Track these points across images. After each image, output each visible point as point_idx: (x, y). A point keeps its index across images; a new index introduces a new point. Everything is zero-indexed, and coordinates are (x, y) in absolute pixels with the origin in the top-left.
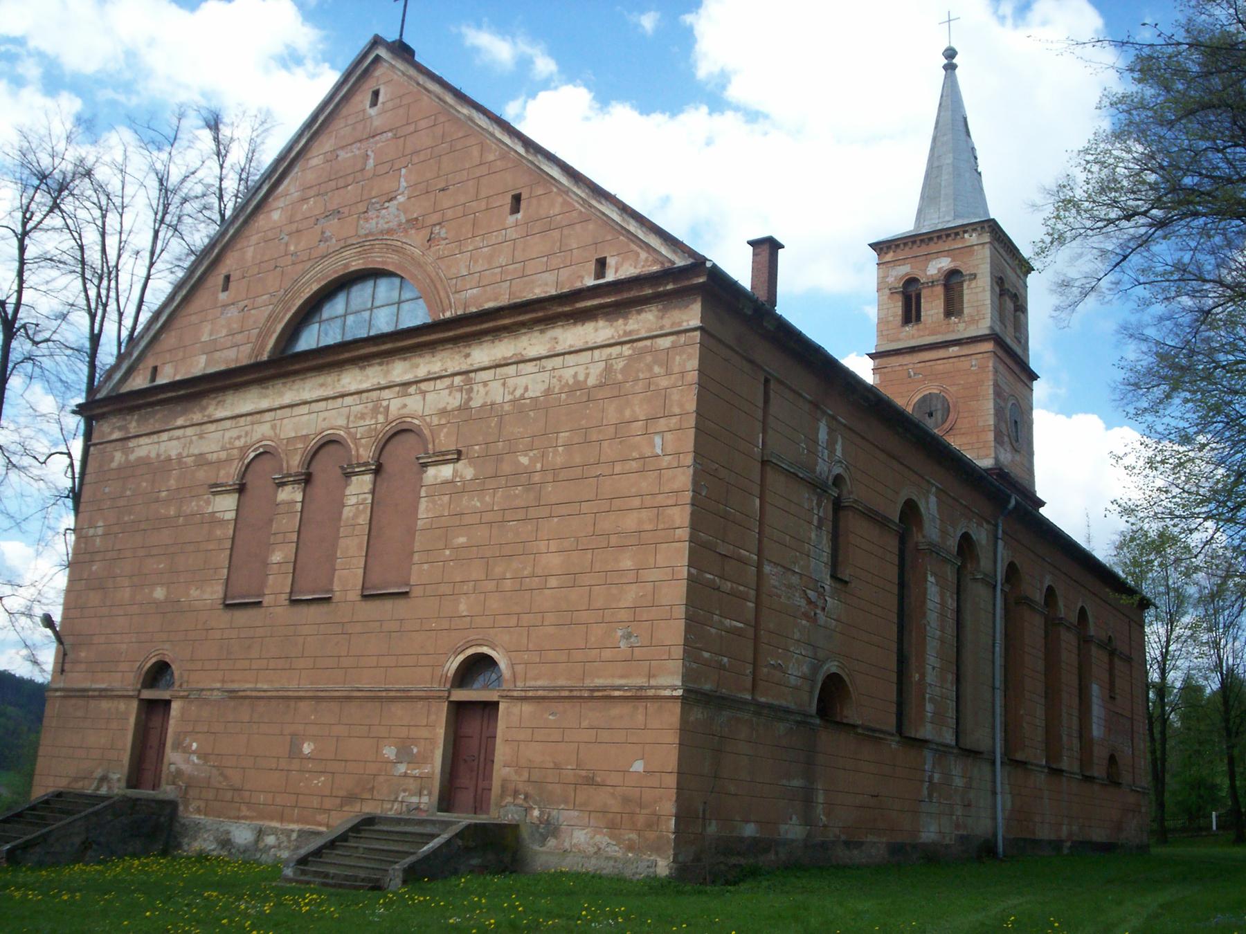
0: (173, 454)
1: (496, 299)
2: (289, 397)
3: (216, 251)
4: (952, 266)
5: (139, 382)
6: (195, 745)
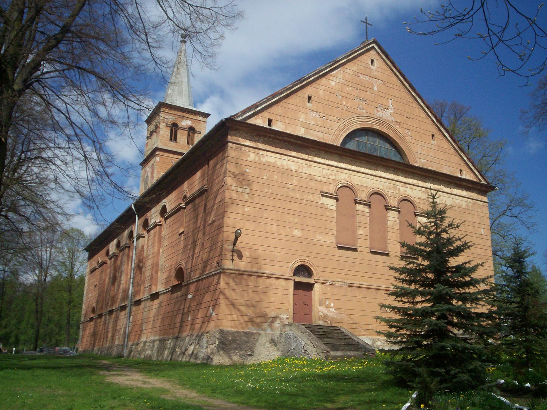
0: (293, 168)
1: (432, 167)
2: (410, 181)
3: (305, 83)
4: (192, 125)
5: (260, 121)
6: (332, 305)
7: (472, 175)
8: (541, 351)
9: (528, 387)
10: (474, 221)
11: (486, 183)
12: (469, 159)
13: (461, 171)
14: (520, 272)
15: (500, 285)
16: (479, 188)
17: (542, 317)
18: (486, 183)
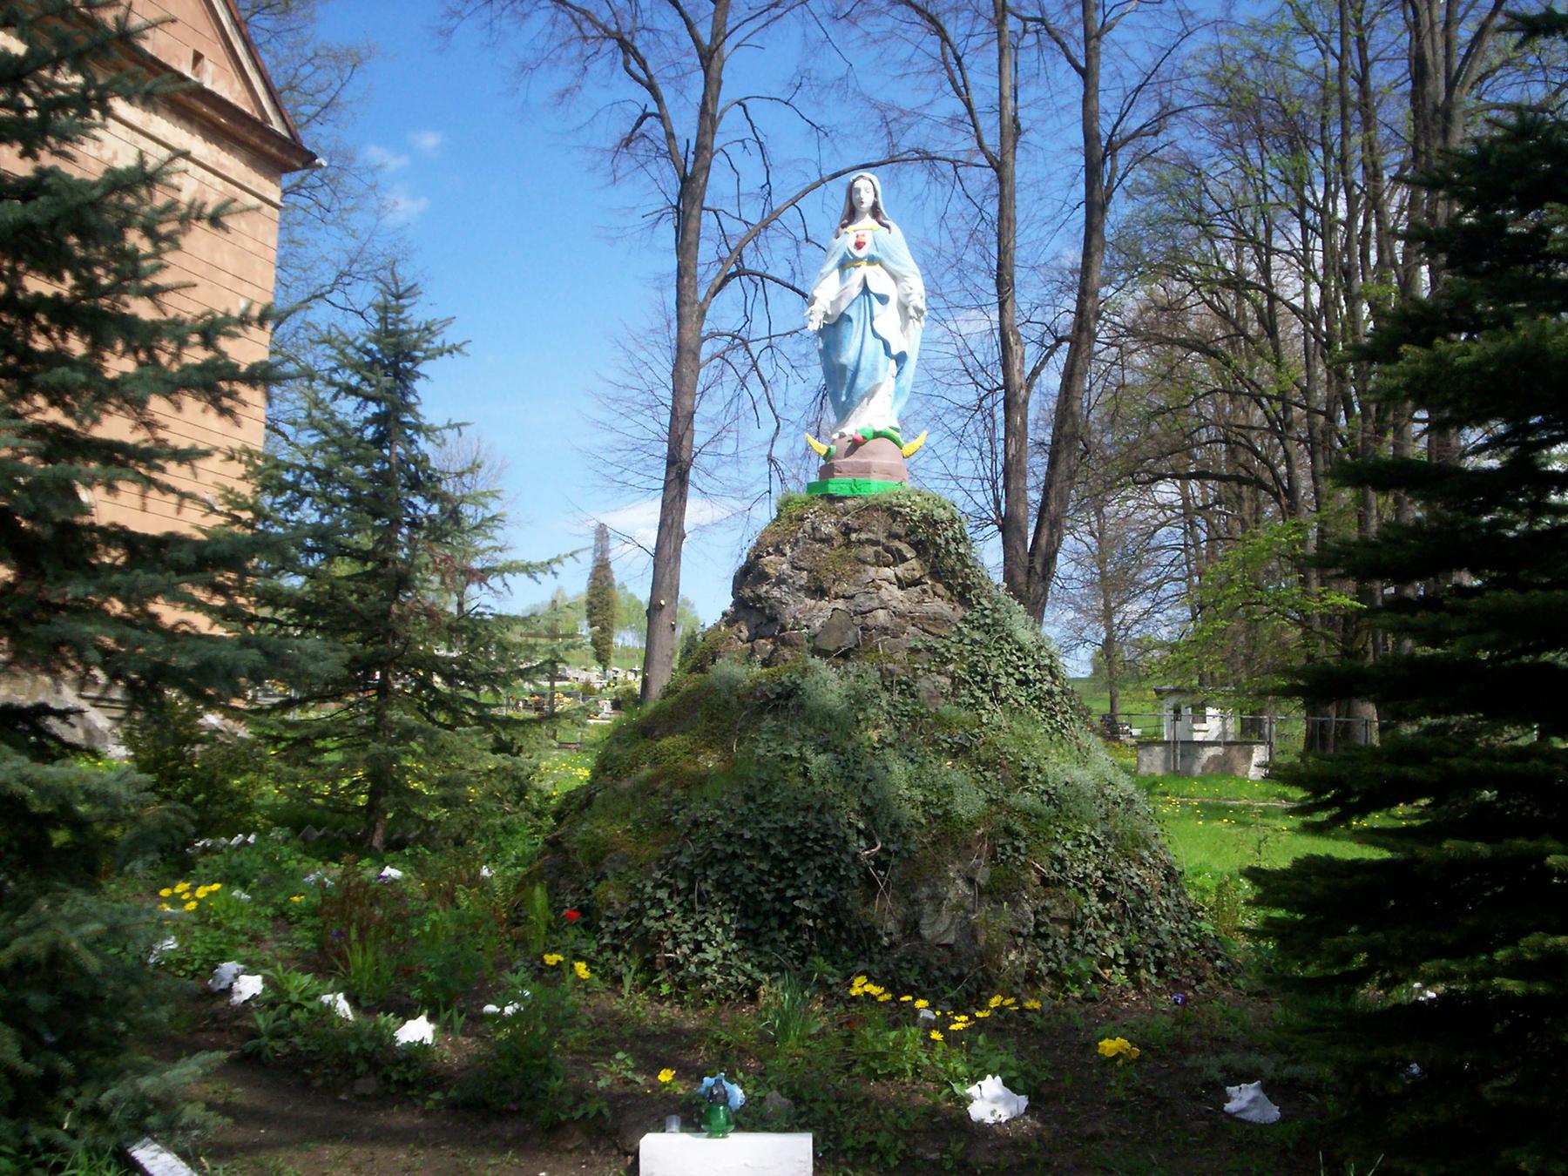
7: (238, 86)
8: (443, 783)
9: (421, 1046)
10: (217, 259)
11: (285, 133)
12: (237, 24)
13: (198, 57)
14: (394, 419)
15: (289, 467)
16: (255, 140)
17: (462, 629)
18: (285, 133)
